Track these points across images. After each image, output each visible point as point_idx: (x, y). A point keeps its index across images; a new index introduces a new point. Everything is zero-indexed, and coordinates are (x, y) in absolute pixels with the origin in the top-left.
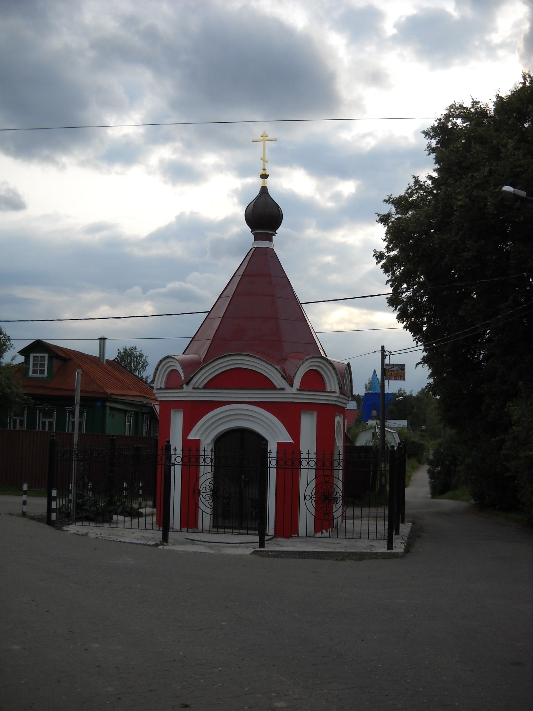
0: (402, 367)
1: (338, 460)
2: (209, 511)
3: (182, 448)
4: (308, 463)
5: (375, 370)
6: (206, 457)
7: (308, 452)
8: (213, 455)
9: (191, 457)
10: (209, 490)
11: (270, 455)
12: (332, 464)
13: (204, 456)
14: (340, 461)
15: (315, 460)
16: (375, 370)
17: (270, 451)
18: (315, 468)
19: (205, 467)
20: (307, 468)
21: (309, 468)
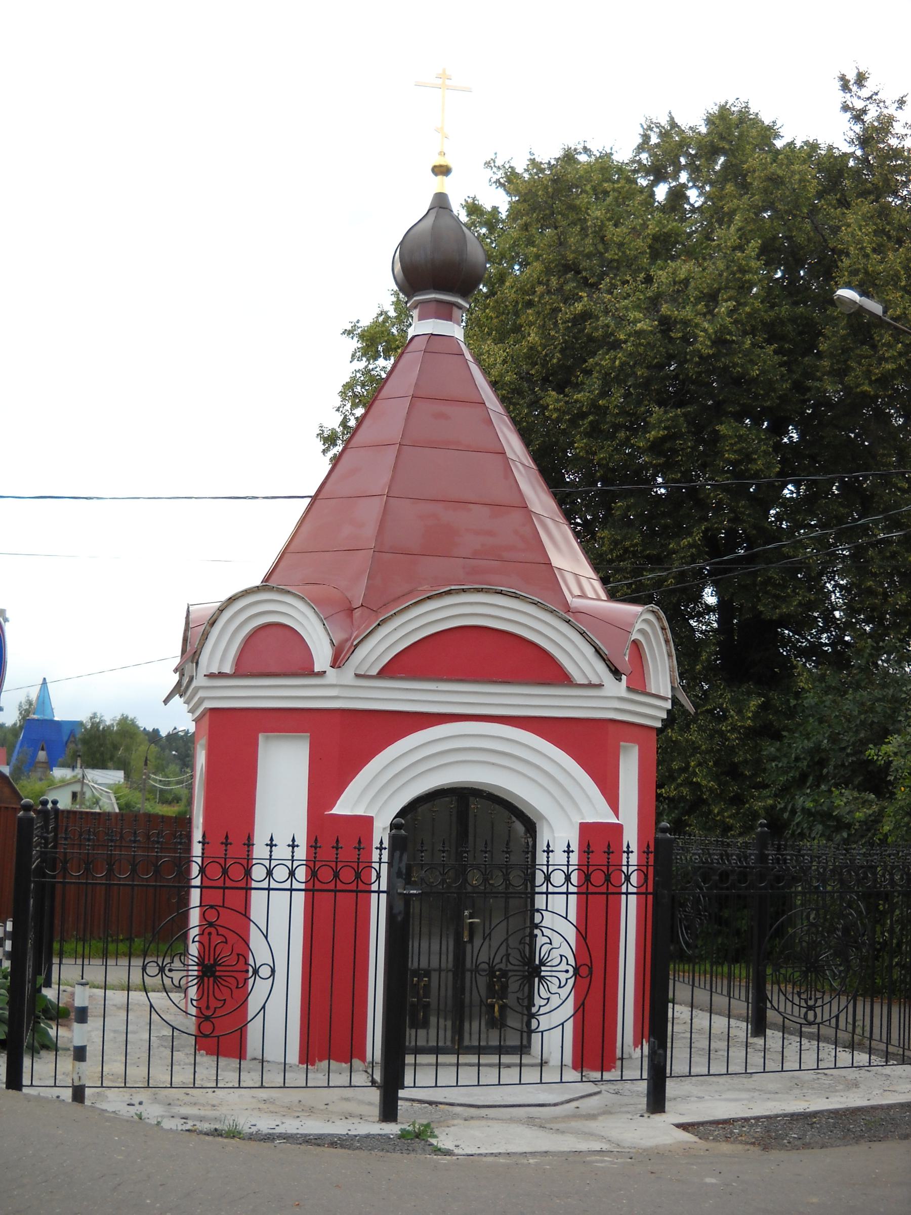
1: (545, 868)
3: (204, 836)
4: (336, 875)
5: (45, 679)
7: (293, 840)
8: (651, 862)
9: (550, 870)
10: (548, 978)
11: (628, 858)
12: (313, 873)
14: (571, 868)
16: (45, 679)
17: (628, 847)
19: (549, 896)
20: (565, 891)
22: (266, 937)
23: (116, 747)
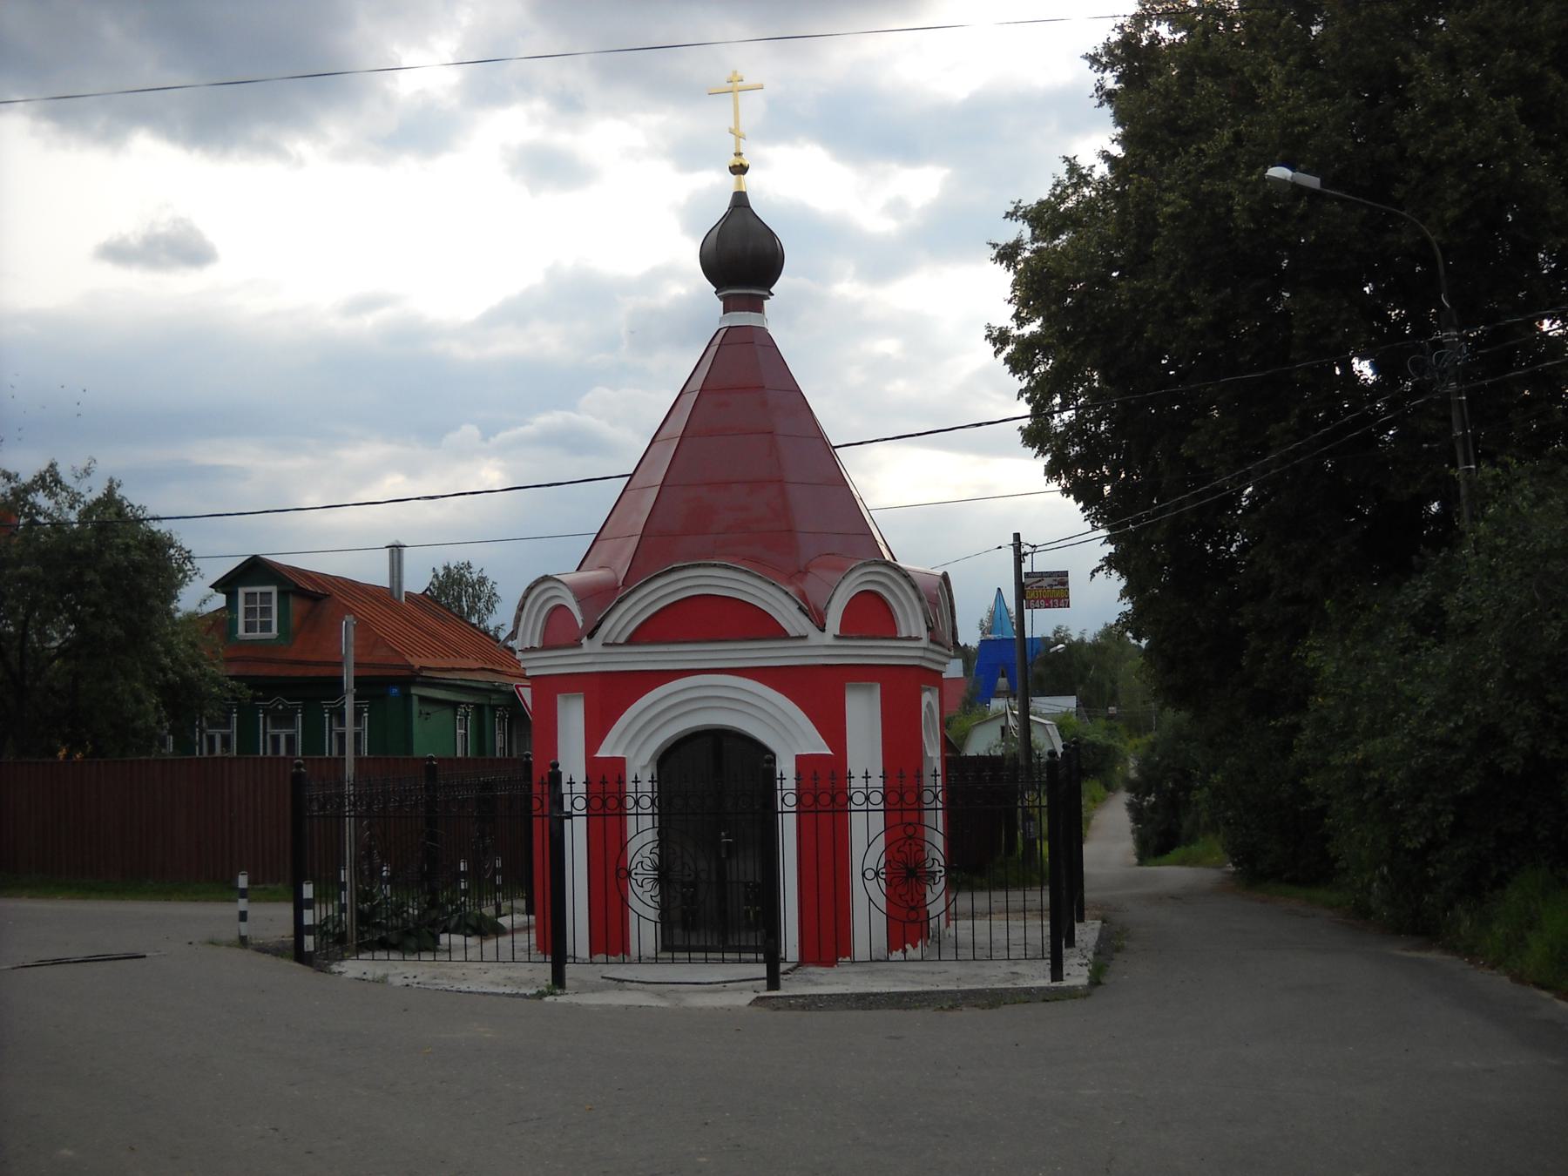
0: (1061, 578)
2: (653, 914)
3: (884, 772)
5: (999, 589)
6: (639, 795)
11: (781, 783)
13: (637, 792)
15: (881, 790)
17: (781, 774)
18: (883, 808)
19: (639, 817)
21: (639, 812)
22: (870, 899)
23: (1087, 667)
